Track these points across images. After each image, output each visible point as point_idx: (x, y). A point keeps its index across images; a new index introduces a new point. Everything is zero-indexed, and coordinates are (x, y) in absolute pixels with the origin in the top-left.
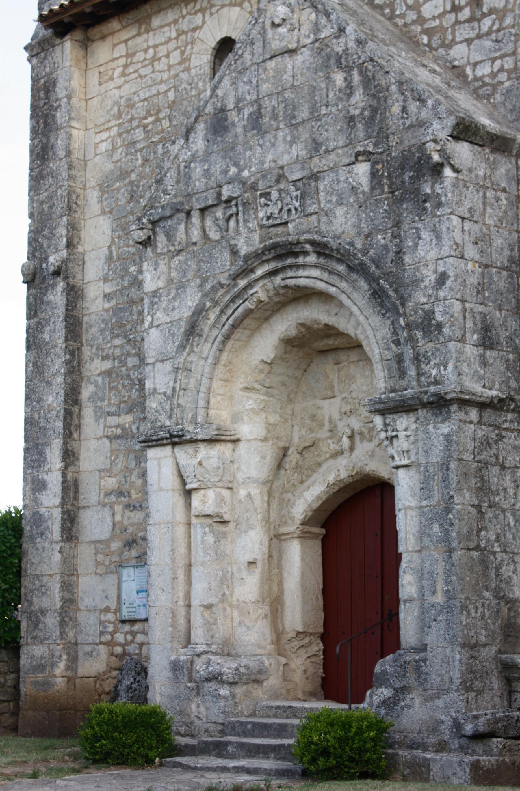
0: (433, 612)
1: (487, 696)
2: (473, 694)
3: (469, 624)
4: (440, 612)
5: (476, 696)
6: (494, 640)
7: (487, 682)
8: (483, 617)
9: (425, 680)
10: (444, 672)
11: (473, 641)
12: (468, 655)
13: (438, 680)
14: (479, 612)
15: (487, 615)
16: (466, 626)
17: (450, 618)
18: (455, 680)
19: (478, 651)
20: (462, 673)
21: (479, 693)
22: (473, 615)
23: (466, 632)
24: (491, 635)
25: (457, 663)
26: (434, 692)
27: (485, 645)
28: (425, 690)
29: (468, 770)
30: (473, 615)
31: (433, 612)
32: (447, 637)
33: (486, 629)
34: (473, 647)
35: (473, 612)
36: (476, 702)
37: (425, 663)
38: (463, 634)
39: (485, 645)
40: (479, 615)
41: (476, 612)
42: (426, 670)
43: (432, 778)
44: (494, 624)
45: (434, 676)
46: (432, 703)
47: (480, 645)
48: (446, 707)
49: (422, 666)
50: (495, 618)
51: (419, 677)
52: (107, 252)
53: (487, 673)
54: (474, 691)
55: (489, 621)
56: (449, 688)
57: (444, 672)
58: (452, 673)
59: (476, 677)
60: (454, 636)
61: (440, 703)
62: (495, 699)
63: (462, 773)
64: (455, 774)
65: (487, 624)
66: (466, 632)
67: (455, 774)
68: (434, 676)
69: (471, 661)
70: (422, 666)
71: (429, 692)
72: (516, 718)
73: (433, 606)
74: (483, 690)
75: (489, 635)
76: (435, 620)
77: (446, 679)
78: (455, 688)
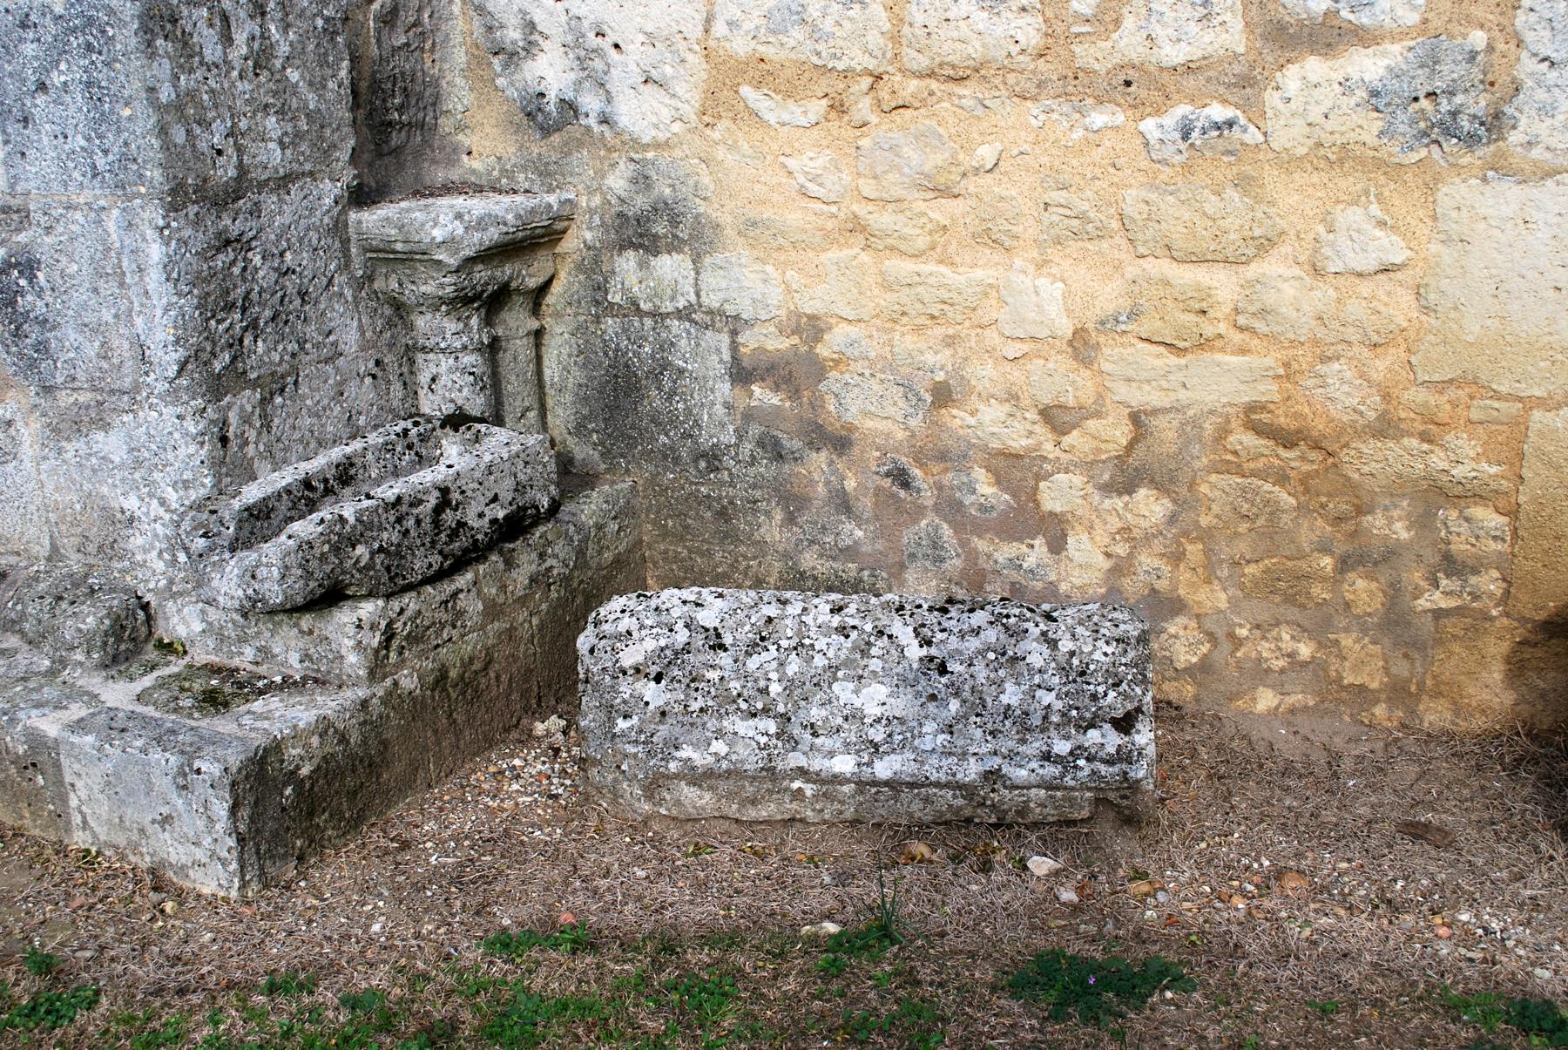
0: (29, 49)
1: (314, 390)
2: (248, 399)
3: (192, 95)
4: (57, 52)
5: (264, 401)
6: (326, 153)
7: (311, 330)
8: (260, 59)
9: (42, 347)
10: (108, 316)
11: (226, 171)
12: (199, 240)
13: (92, 349)
14: (240, 38)
15: (284, 49)
16: (178, 107)
17: (102, 76)
18: (156, 353)
19: (256, 211)
20: (181, 323)
21: (276, 385)
22: (212, 52)
23: (179, 135)
24: (308, 135)
25: (154, 278)
26: (83, 398)
27: (284, 182)
28: (48, 390)
29: (221, 809)
30: (212, 52)
31: (29, 49)
32: (101, 162)
33: (281, 112)
34: (224, 198)
35: (207, 40)
36: (267, 426)
37: (32, 279)
38: (167, 146)
39: (284, 182)
40: (240, 48)
41: (227, 39)
42: (40, 308)
43: (77, 819)
44: (318, 86)
45: (72, 335)
46: (80, 444)
47: (262, 185)
48: (138, 464)
49: (21, 292)
50: (323, 62)
51: (17, 334)
52: (646, 140)
53: (303, 295)
54: (254, 385)
55: (293, 75)
56: (136, 388)
57: (108, 316)
58: (139, 321)
59: (253, 325)
60: (126, 158)
61: (111, 444)
62: (351, 389)
63: (201, 824)
64: (166, 820)
65: (283, 88)
66: (179, 135)
67: (166, 820)
68: (72, 335)
69: (221, 260)
70: (21, 292)
71: (65, 399)
72: (433, 500)
73: (24, 26)
74: (295, 371)
75: (298, 135)
76: (42, 87)
77: (122, 347)
78: (162, 386)
